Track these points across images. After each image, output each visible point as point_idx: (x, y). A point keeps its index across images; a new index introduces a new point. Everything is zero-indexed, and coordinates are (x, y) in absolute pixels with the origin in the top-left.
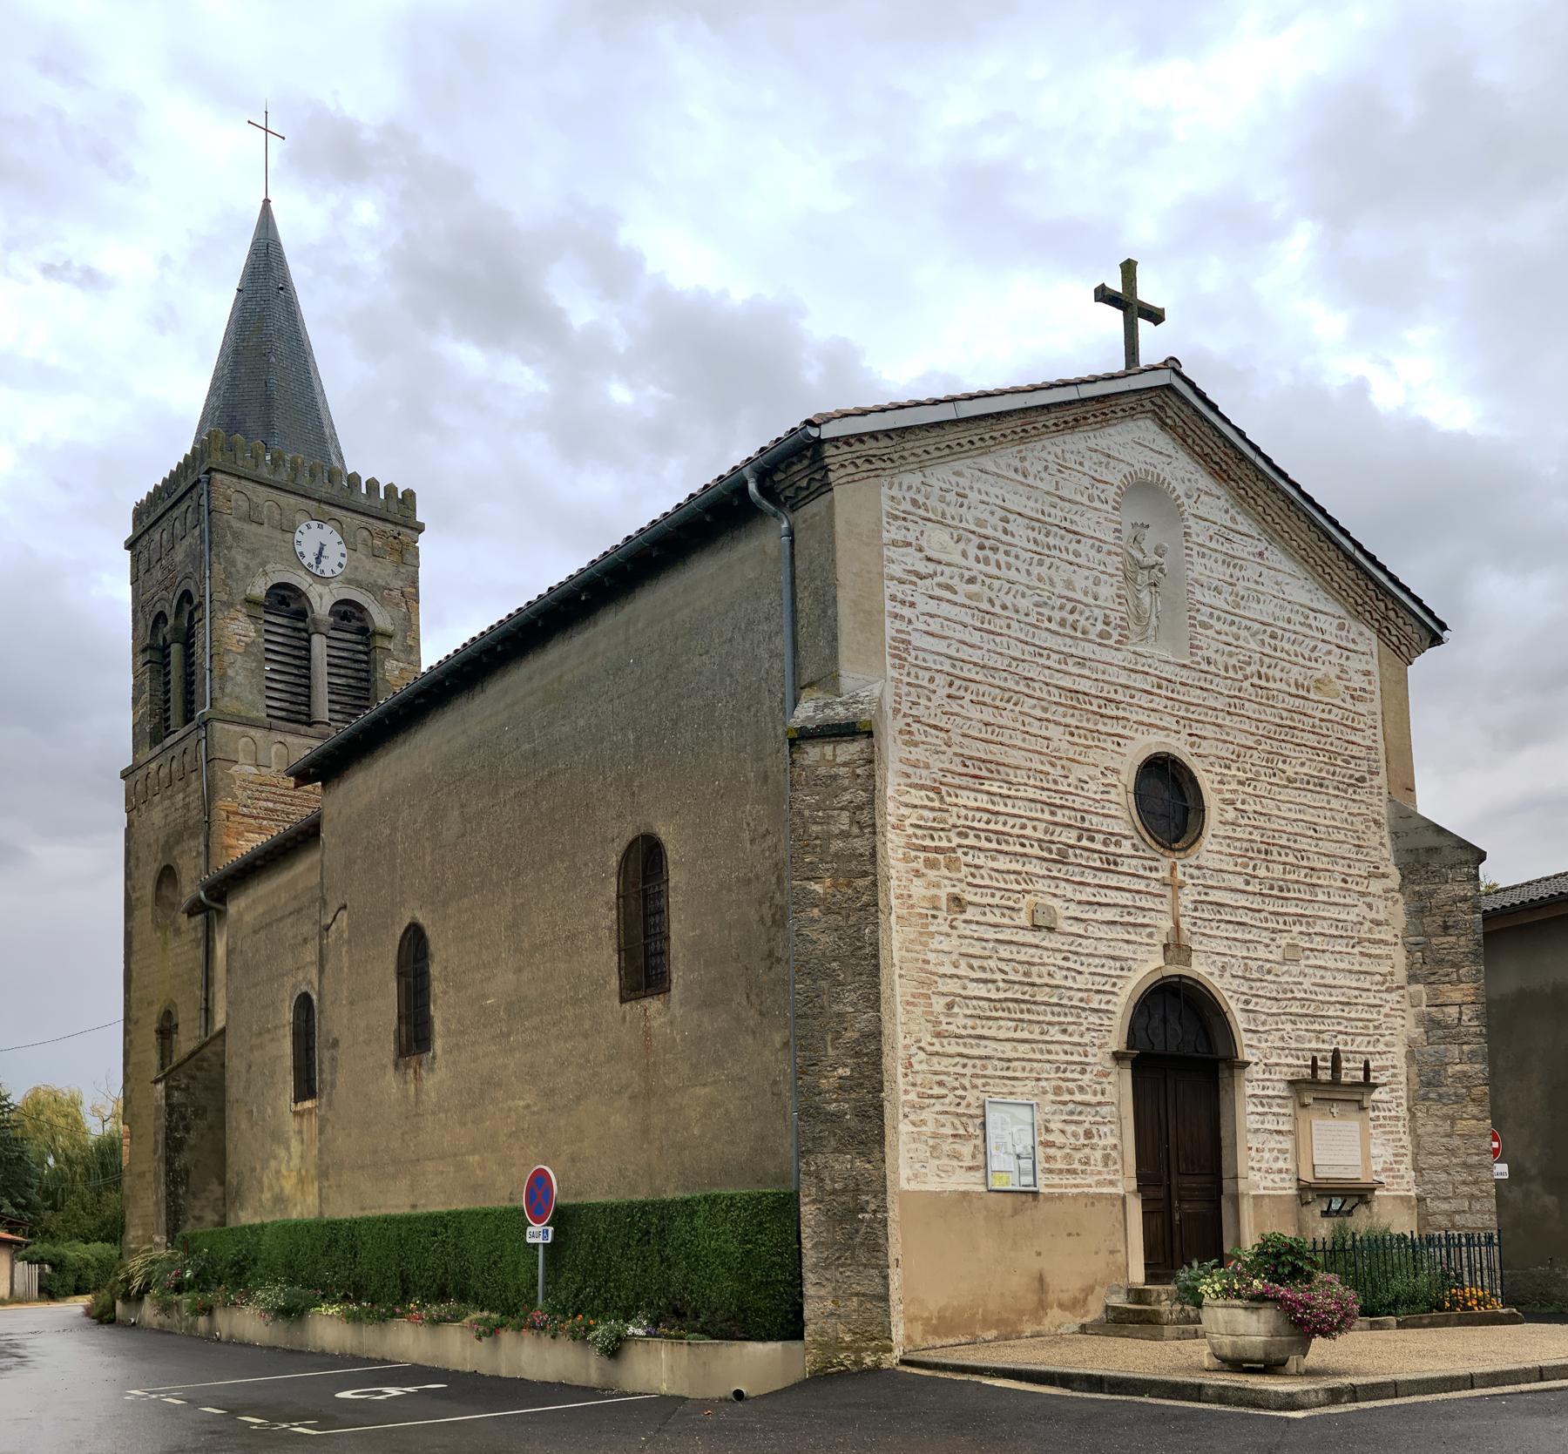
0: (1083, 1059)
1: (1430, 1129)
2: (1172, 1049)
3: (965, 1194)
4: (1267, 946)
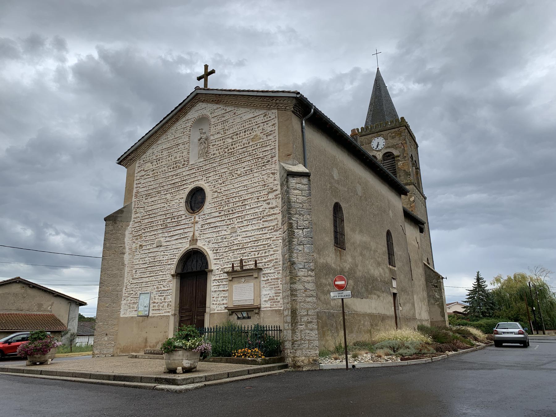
2: (199, 269)
3: (132, 317)
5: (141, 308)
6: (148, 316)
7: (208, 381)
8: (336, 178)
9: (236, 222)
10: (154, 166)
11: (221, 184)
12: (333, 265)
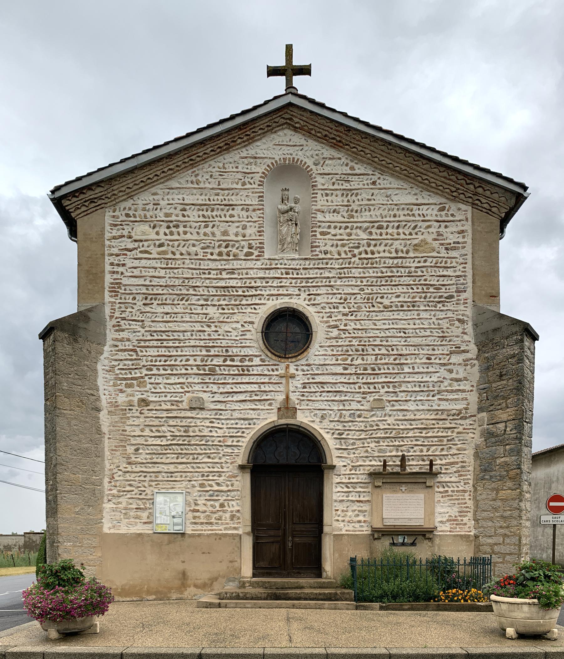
0: (221, 470)
1: (484, 496)
2: (293, 462)
3: (140, 535)
11: (346, 315)
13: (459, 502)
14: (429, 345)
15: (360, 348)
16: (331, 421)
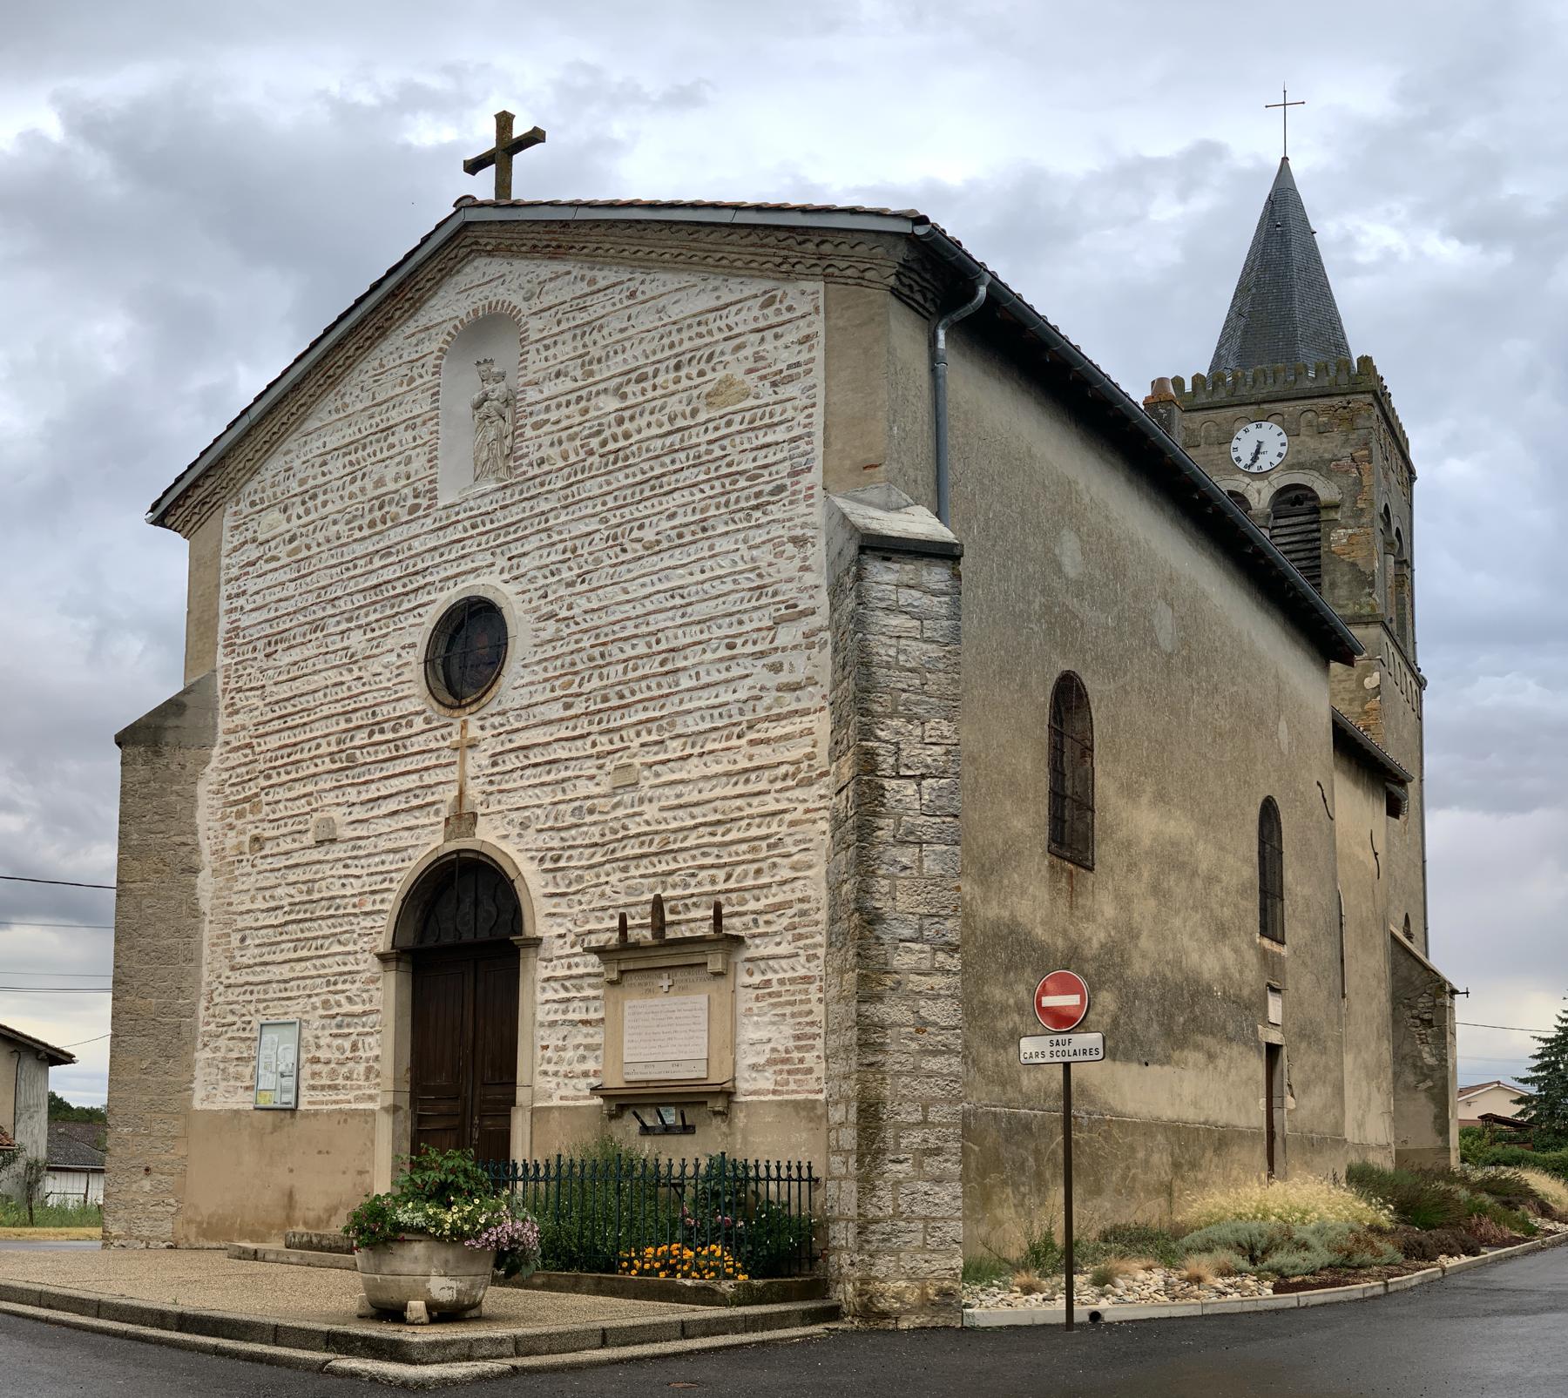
2: (484, 935)
3: (237, 1112)
4: (592, 778)
5: (267, 1081)
6: (293, 1111)
7: (527, 1355)
8: (1071, 571)
9: (637, 742)
10: (295, 522)
11: (571, 584)
12: (1039, 931)
13: (796, 1009)
14: (731, 615)
15: (596, 652)
16: (541, 831)
